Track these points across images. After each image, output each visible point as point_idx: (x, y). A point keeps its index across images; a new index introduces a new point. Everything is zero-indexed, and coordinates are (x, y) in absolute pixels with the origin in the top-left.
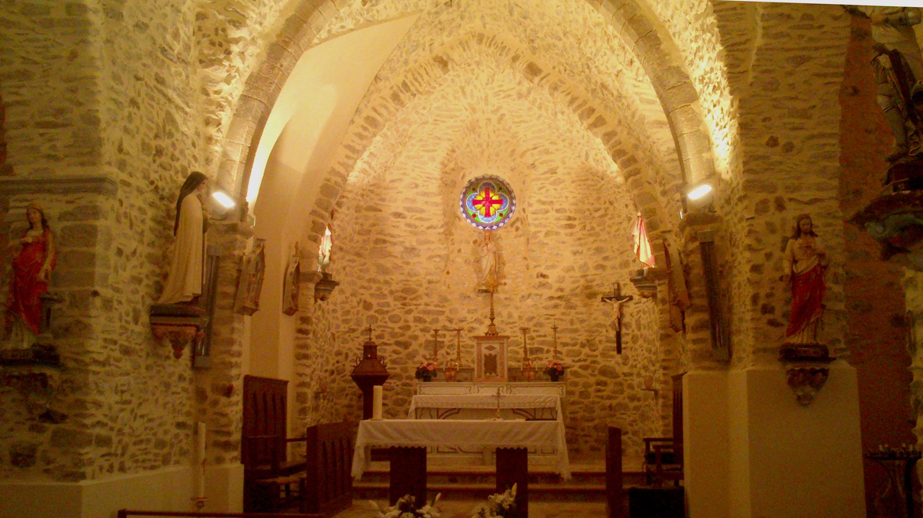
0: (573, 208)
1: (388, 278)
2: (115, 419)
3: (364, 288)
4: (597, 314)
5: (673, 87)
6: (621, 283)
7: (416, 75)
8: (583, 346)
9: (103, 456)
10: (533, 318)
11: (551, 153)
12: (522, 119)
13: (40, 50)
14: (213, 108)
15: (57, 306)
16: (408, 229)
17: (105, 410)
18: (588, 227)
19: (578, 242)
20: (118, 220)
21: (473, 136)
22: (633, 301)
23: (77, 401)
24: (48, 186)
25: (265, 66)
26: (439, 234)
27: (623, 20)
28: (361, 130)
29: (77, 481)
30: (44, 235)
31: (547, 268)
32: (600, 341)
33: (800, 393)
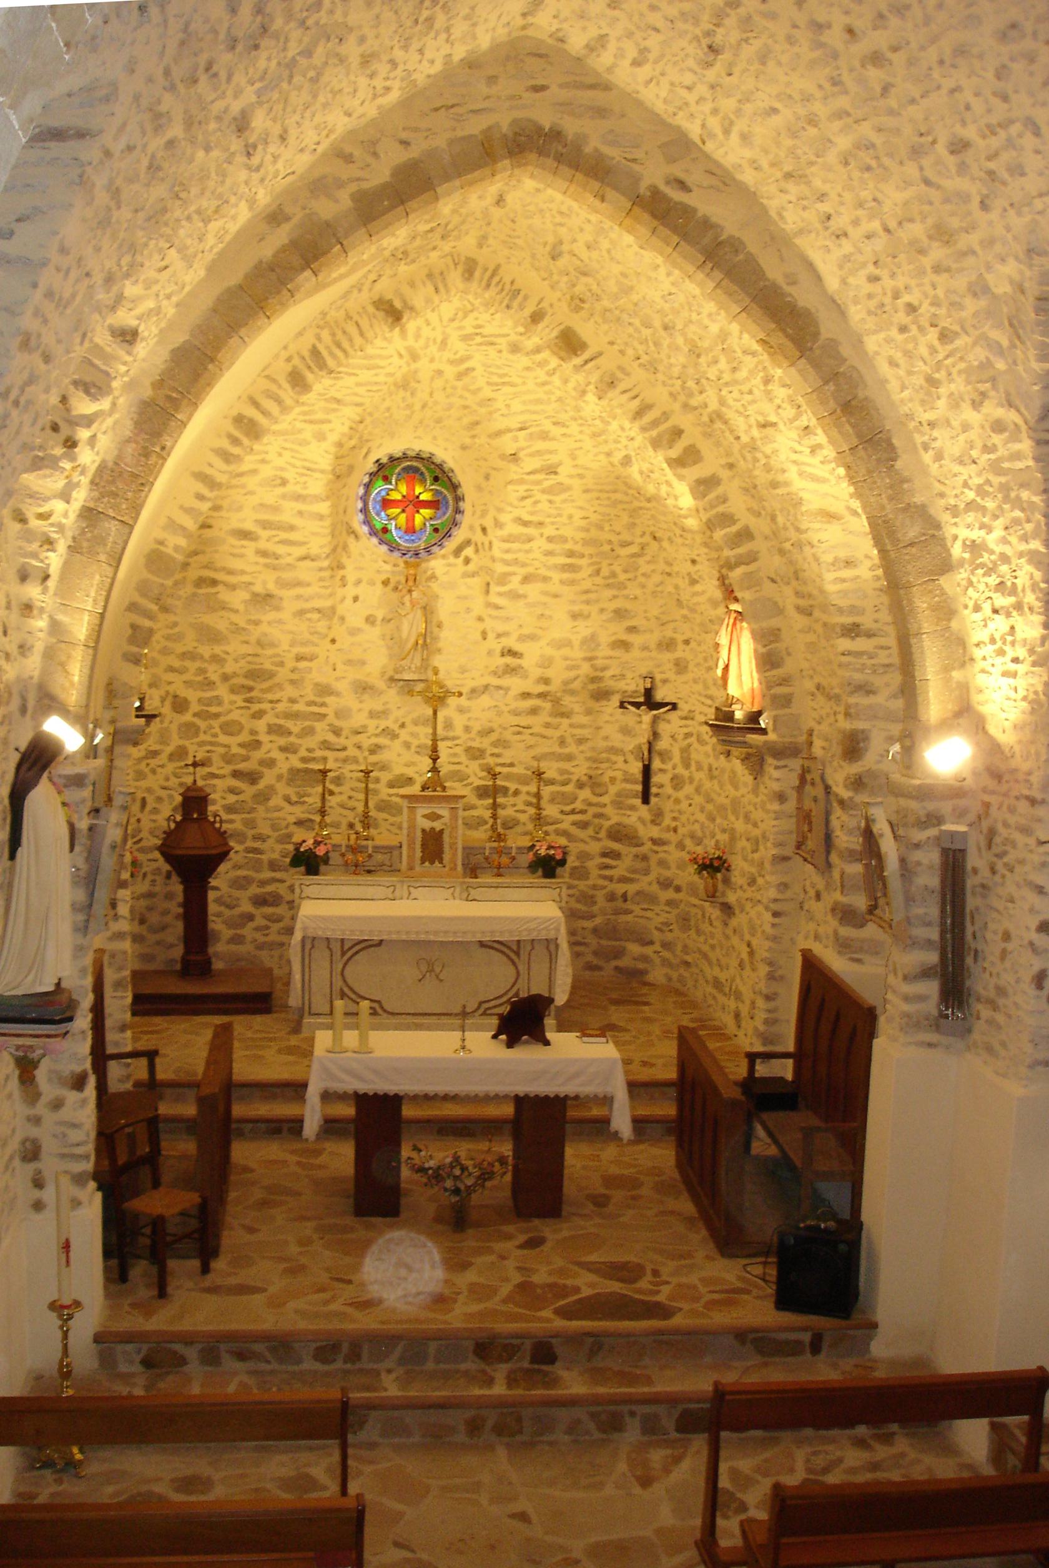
0: (580, 535)
1: (218, 650)
3: (171, 669)
4: (610, 730)
5: (911, 545)
6: (658, 677)
7: (340, 336)
8: (581, 785)
10: (491, 731)
11: (553, 439)
12: (506, 379)
14: (35, 546)
16: (262, 560)
18: (605, 572)
19: (585, 597)
21: (401, 393)
22: (678, 713)
25: (130, 449)
26: (321, 569)
27: (832, 404)
28: (225, 444)
31: (522, 638)
32: (613, 780)
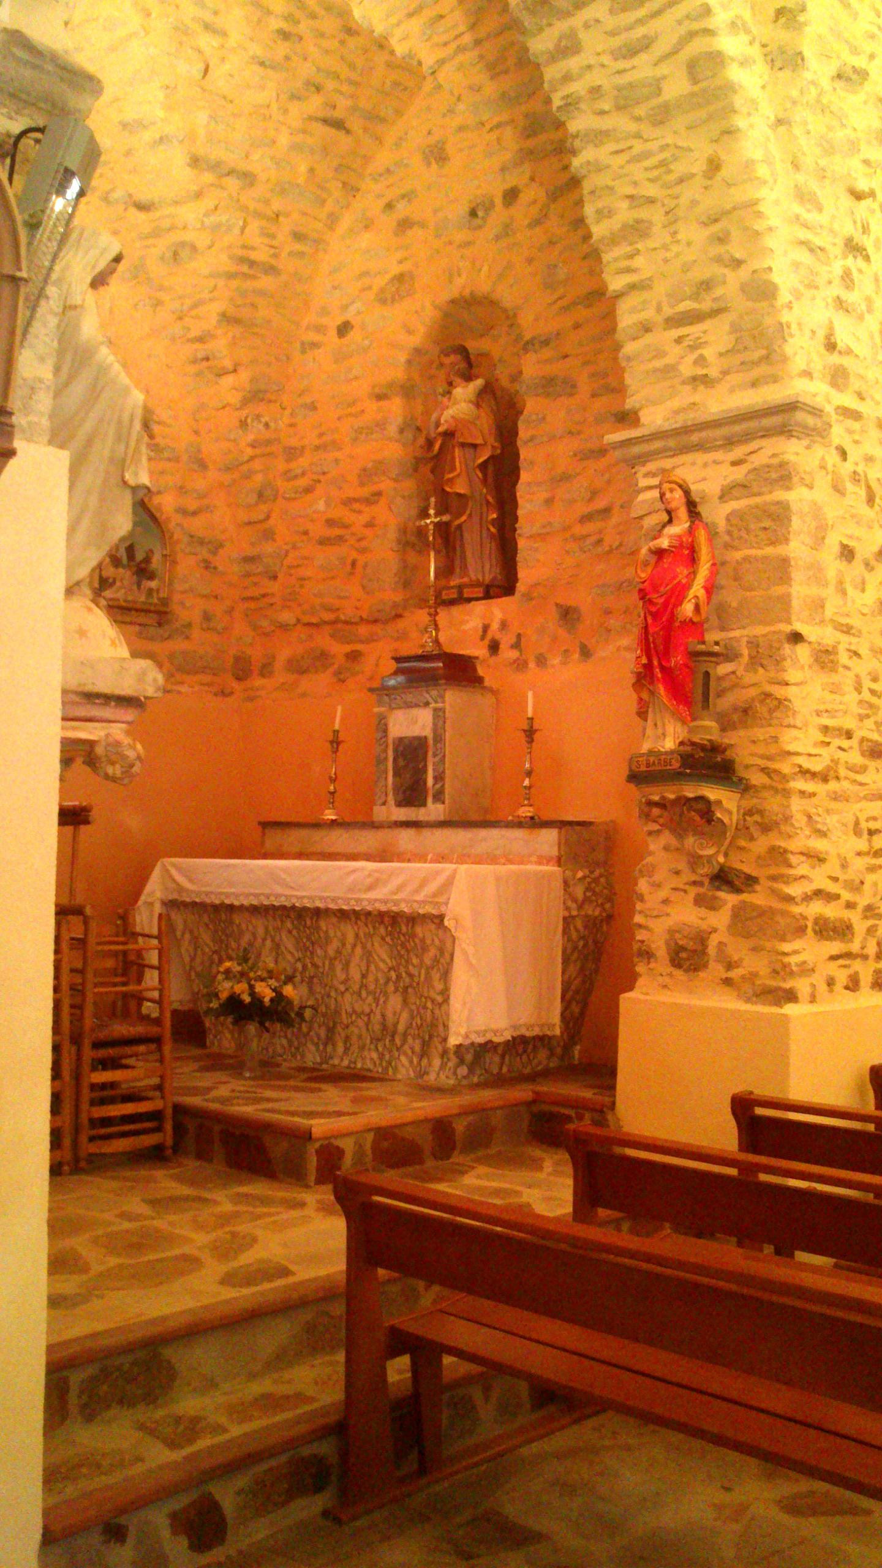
2: (857, 886)
9: (833, 958)
13: (656, 173)
15: (723, 669)
17: (832, 867)
20: (838, 489)
23: (773, 849)
24: (695, 438)
29: (778, 1003)
30: (691, 531)
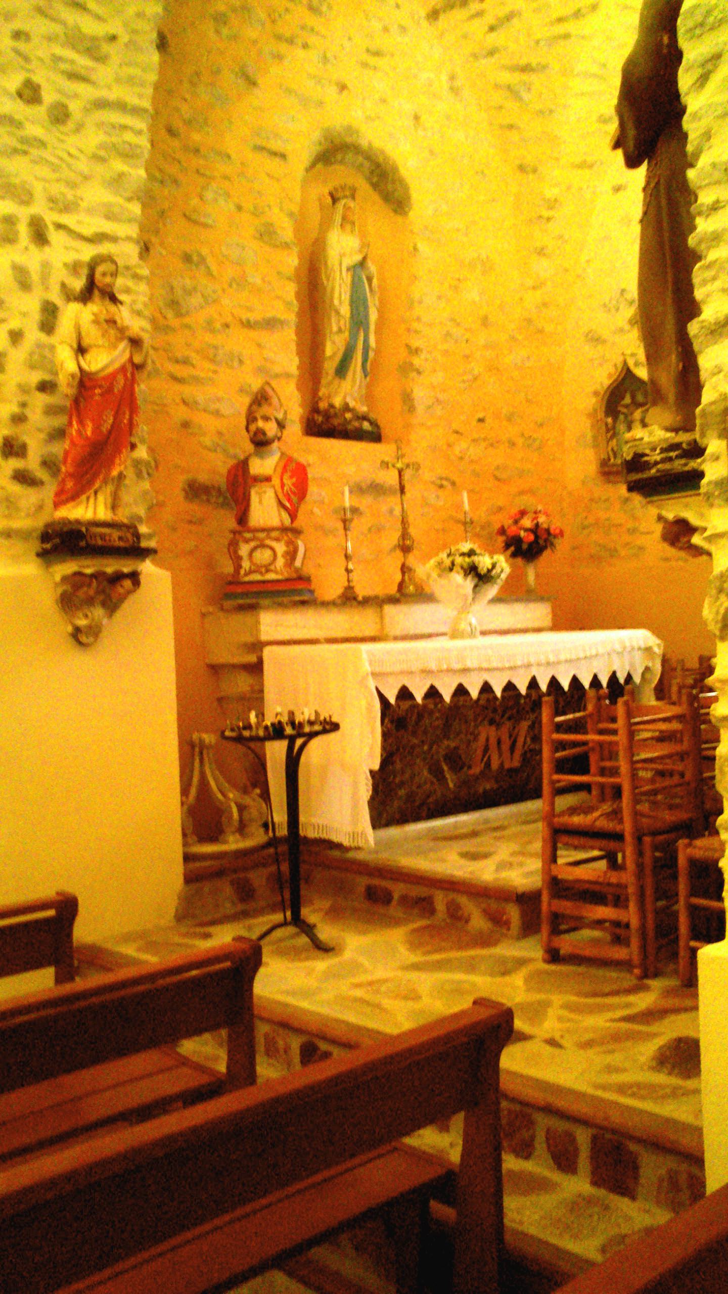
33: (82, 622)
